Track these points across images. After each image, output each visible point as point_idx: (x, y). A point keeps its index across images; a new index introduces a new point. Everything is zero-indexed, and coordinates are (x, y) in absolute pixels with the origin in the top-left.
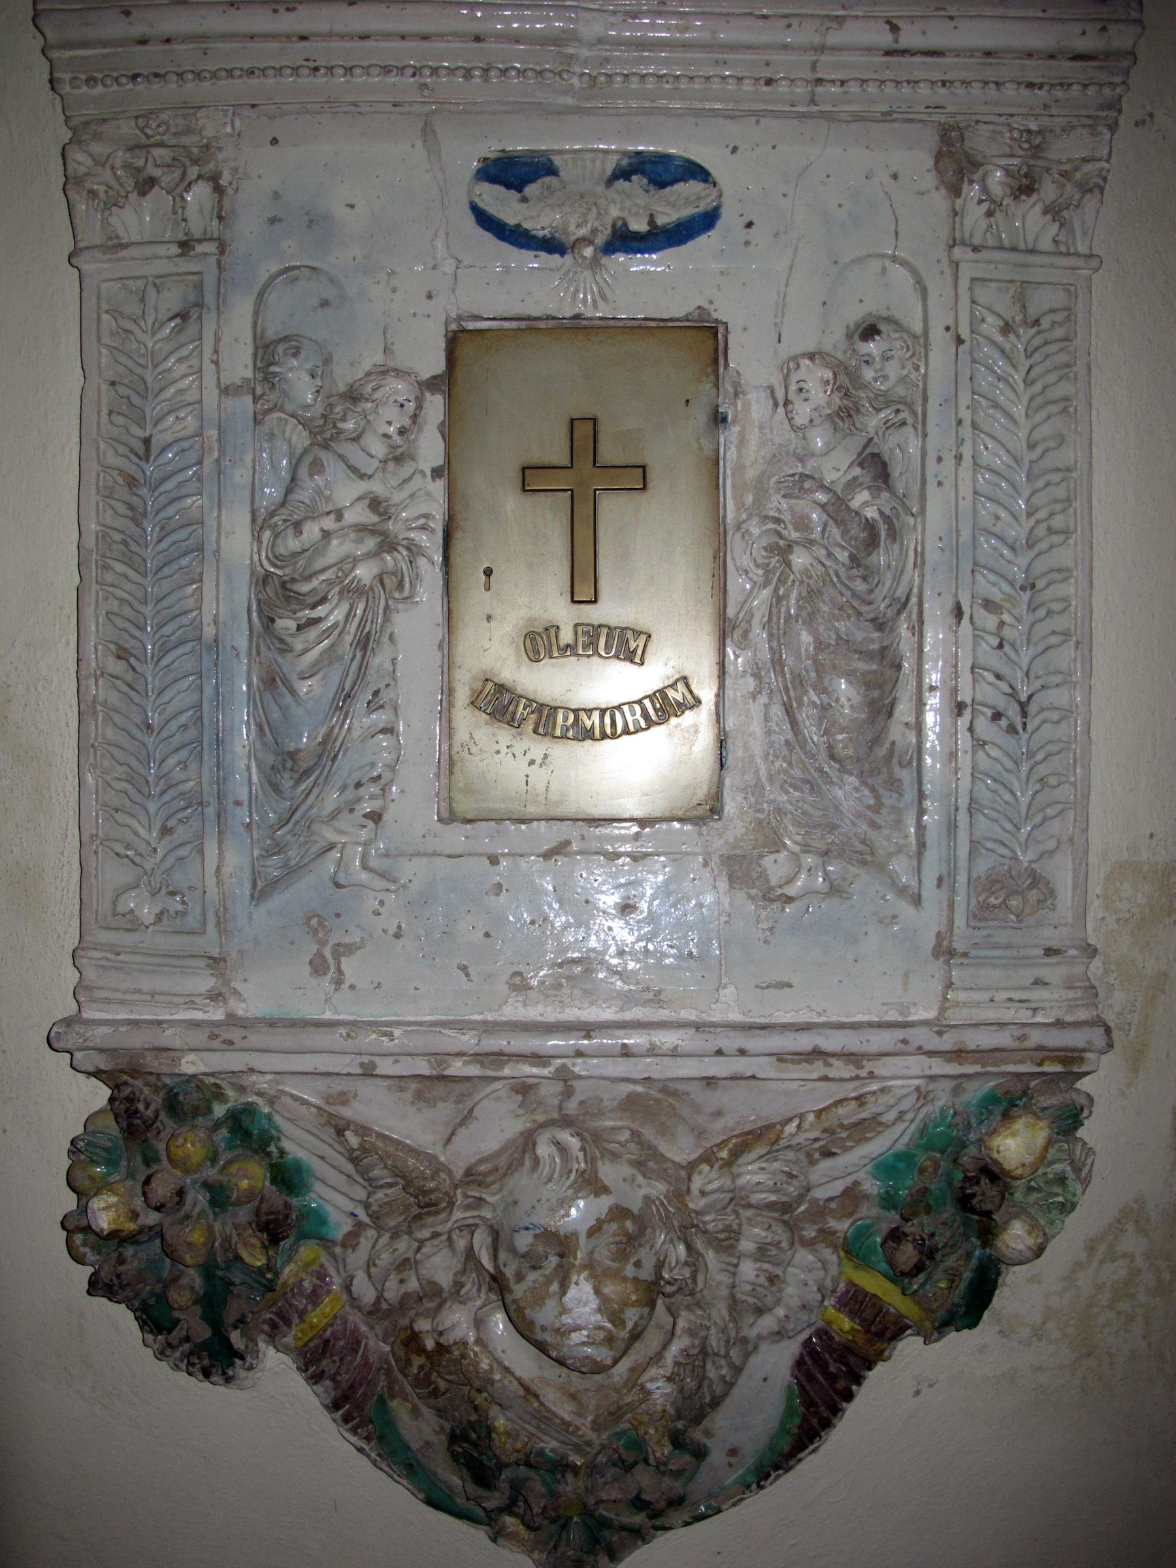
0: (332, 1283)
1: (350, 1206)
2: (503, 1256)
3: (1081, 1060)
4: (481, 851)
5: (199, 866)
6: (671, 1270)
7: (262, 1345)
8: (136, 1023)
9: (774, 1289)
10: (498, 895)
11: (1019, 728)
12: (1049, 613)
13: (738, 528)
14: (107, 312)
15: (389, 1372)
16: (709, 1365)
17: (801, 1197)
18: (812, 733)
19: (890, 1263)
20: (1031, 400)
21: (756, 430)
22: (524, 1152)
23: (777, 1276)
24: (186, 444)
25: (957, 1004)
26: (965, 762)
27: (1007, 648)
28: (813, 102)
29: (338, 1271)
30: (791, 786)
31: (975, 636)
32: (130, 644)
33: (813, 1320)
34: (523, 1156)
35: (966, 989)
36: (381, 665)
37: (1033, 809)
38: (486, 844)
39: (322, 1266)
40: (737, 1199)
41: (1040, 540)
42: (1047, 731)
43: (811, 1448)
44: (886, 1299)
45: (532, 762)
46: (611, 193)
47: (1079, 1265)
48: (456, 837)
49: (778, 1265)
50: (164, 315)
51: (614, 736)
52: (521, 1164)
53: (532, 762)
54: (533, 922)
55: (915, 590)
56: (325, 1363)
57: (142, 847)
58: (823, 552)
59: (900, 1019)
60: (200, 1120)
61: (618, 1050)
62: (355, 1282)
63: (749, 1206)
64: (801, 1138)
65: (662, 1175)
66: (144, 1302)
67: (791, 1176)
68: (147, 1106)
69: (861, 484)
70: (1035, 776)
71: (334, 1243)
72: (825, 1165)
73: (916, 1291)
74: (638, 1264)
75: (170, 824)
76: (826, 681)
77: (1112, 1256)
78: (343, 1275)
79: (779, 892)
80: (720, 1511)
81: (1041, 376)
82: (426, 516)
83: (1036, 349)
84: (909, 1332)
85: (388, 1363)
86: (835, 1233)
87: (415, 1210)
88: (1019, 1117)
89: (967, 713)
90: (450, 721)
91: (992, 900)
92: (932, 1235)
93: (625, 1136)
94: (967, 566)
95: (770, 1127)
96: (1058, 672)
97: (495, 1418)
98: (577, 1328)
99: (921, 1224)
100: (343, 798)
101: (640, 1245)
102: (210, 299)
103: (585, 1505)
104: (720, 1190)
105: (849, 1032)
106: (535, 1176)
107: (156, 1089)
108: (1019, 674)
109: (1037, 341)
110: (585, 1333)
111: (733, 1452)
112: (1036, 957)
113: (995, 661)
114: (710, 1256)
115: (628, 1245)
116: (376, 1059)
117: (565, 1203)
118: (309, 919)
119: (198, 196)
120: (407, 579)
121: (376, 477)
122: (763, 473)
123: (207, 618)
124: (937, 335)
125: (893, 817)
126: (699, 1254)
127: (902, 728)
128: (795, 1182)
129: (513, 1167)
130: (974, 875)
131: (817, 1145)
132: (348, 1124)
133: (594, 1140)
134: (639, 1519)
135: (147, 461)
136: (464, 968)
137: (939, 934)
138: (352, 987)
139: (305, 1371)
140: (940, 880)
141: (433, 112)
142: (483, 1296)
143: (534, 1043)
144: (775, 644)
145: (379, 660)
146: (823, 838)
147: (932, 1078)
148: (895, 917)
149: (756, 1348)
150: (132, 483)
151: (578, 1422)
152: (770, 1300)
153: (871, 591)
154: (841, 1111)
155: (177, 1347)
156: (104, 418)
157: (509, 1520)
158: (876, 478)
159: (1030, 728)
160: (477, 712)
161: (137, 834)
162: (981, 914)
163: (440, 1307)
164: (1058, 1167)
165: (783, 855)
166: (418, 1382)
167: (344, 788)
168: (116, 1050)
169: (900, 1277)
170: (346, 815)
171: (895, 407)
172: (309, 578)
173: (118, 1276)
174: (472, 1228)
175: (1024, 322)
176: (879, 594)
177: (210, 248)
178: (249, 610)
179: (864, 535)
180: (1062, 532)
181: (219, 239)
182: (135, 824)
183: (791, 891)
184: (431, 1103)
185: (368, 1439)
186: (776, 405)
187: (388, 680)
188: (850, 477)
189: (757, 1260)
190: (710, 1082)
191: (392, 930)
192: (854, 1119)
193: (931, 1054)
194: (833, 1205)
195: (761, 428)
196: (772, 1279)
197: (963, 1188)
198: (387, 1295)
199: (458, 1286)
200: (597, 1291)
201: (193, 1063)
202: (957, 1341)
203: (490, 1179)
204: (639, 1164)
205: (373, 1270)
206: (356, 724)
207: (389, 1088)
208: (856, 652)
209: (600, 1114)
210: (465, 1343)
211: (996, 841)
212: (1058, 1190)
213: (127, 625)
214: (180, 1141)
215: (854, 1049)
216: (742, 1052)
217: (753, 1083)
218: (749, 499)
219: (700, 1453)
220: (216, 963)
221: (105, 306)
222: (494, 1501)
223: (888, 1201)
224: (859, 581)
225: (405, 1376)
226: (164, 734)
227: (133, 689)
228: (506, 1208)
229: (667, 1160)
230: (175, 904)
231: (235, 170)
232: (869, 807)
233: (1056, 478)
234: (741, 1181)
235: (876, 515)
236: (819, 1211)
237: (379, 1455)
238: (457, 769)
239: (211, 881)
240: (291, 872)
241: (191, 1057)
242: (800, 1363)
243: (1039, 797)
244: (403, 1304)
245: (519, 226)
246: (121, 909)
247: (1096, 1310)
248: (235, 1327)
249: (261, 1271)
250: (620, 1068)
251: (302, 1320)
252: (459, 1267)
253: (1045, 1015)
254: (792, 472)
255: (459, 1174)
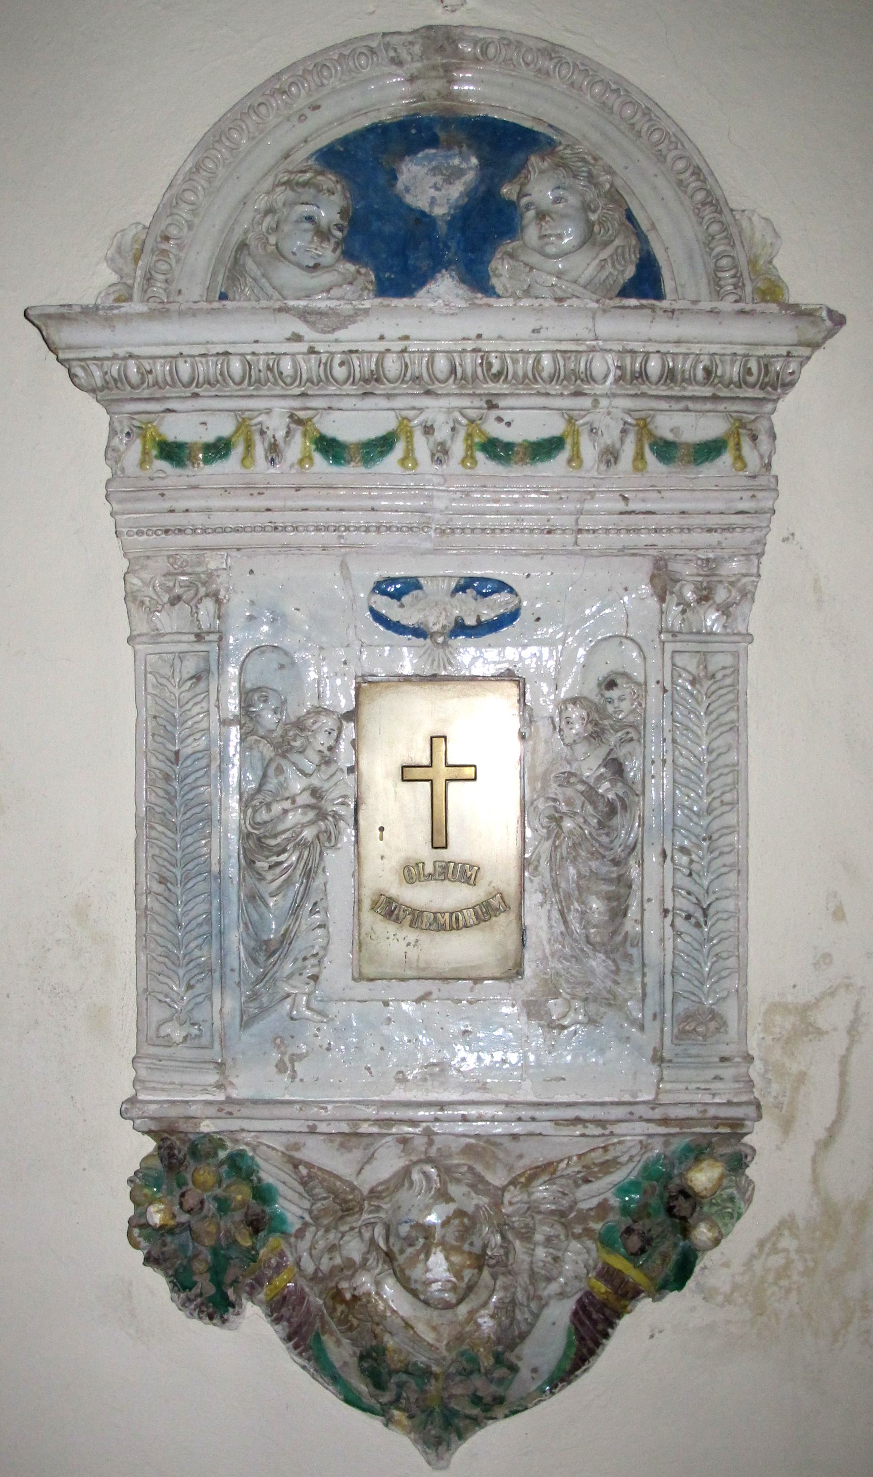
0: (288, 1260)
1: (299, 1212)
2: (392, 1240)
3: (742, 1126)
4: (378, 998)
5: (209, 1008)
6: (492, 1250)
7: (244, 1301)
8: (173, 1102)
9: (558, 1265)
10: (388, 1024)
11: (703, 924)
12: (721, 854)
13: (532, 804)
14: (150, 673)
15: (322, 1317)
16: (517, 1311)
17: (571, 1208)
18: (576, 926)
19: (625, 1248)
20: (710, 724)
21: (543, 744)
22: (405, 1177)
23: (558, 1257)
24: (200, 755)
25: (666, 1091)
26: (669, 944)
27: (694, 875)
28: (576, 543)
29: (292, 1253)
30: (564, 959)
31: (674, 869)
32: (168, 874)
33: (583, 1286)
34: (403, 1181)
35: (671, 1082)
36: (318, 886)
37: (711, 974)
38: (383, 994)
39: (282, 1250)
40: (532, 1208)
41: (715, 809)
42: (720, 925)
43: (583, 1368)
44: (625, 1272)
45: (409, 944)
46: (454, 601)
47: (753, 1257)
48: (363, 989)
49: (559, 1250)
50: (186, 676)
51: (458, 928)
52: (403, 1185)
53: (409, 944)
54: (409, 1041)
55: (640, 840)
56: (284, 1310)
57: (175, 996)
58: (582, 820)
59: (631, 1100)
60: (210, 1161)
61: (460, 1118)
62: (303, 1260)
63: (540, 1212)
64: (569, 1171)
65: (486, 1193)
66: (176, 1271)
67: (564, 1194)
68: (180, 1152)
69: (605, 778)
70: (712, 954)
71: (290, 1235)
72: (585, 1188)
73: (641, 1265)
74: (471, 1244)
75: (192, 982)
76: (584, 897)
77: (775, 1251)
78: (295, 1254)
79: (558, 1023)
80: (526, 1409)
81: (716, 709)
82: (345, 796)
83: (713, 693)
84: (643, 1294)
85: (322, 1312)
86: (594, 1230)
87: (340, 1213)
88: (704, 1160)
89: (670, 917)
90: (359, 919)
91: (687, 1028)
92: (650, 1230)
93: (465, 1169)
94: (669, 827)
95: (550, 1164)
96: (729, 889)
97: (388, 1342)
98: (436, 1281)
99: (644, 1225)
100: (296, 966)
101: (473, 1234)
102: (214, 667)
103: (442, 1398)
104: (521, 1201)
105: (598, 1107)
106: (411, 1192)
107: (184, 1142)
108: (702, 892)
109: (714, 687)
110: (440, 1283)
111: (535, 1370)
112: (715, 1062)
113: (686, 883)
114: (517, 1243)
115: (466, 1233)
116: (317, 1123)
117: (428, 1209)
118: (275, 1039)
119: (208, 606)
120: (333, 835)
121: (315, 775)
122: (547, 769)
123: (214, 861)
124: (652, 685)
125: (627, 977)
126: (510, 1242)
127: (632, 923)
128: (567, 1198)
129: (398, 1188)
130: (676, 1012)
131: (579, 1176)
132: (300, 1162)
133: (446, 1172)
134: (475, 1411)
135: (177, 765)
136: (368, 1069)
137: (655, 1049)
138: (302, 1080)
139: (270, 1316)
140: (655, 1016)
141: (346, 554)
142: (380, 1266)
143: (410, 1114)
144: (554, 874)
145: (318, 883)
146: (583, 990)
147: (650, 1136)
148: (628, 1038)
149: (547, 1304)
150: (167, 778)
151: (438, 1345)
152: (555, 1273)
153: (612, 842)
154: (593, 1154)
155: (194, 1300)
156: (150, 737)
157: (396, 1413)
158: (614, 774)
159: (709, 923)
160: (375, 914)
161: (172, 989)
162: (681, 1035)
163: (353, 1275)
164: (729, 1191)
165: (559, 1001)
166: (340, 1322)
167: (296, 960)
168: (161, 1118)
169: (633, 1256)
170: (296, 976)
171: (626, 731)
172: (275, 836)
173: (163, 1253)
174: (373, 1225)
175: (706, 676)
176: (617, 843)
177: (213, 637)
178: (239, 855)
179: (606, 809)
180: (730, 804)
181: (219, 632)
182: (171, 983)
183: (566, 1022)
184: (350, 1150)
185: (309, 1359)
186: (555, 728)
187: (322, 896)
188: (598, 773)
189: (546, 1247)
190: (515, 1137)
191: (326, 1046)
192: (601, 1160)
193: (649, 1121)
194: (592, 1213)
195: (546, 742)
196: (556, 1259)
197: (668, 1203)
198: (322, 1267)
199: (365, 1260)
200: (447, 1258)
201: (208, 1126)
202: (672, 1298)
203: (384, 1195)
204: (473, 1186)
205: (314, 1252)
206: (303, 921)
207: (324, 1141)
208: (602, 879)
209: (450, 1156)
210: (369, 1294)
211: (690, 992)
212: (729, 1205)
213: (166, 864)
214: (202, 1172)
215: (601, 1118)
216: (533, 1119)
217: (540, 1137)
218: (539, 785)
219: (514, 1369)
220: (220, 1066)
221: (149, 669)
222: (386, 1398)
223: (625, 1210)
224: (604, 837)
225: (332, 1318)
226: (188, 929)
227: (169, 902)
228: (394, 1211)
229: (490, 1184)
230: (194, 1030)
231: (227, 590)
232: (612, 972)
233: (726, 770)
234: (534, 1197)
235: (614, 797)
236: (583, 1217)
237: (315, 1370)
238: (364, 947)
239: (216, 1016)
240: (264, 1010)
241: (207, 1122)
242: (575, 1314)
243: (717, 965)
244: (333, 1271)
245: (398, 622)
246: (162, 1033)
247: (766, 1285)
248: (231, 1285)
249: (249, 1250)
250: (460, 1128)
251: (270, 1283)
252: (365, 1249)
253: (721, 1098)
254: (563, 771)
255: (365, 1192)
